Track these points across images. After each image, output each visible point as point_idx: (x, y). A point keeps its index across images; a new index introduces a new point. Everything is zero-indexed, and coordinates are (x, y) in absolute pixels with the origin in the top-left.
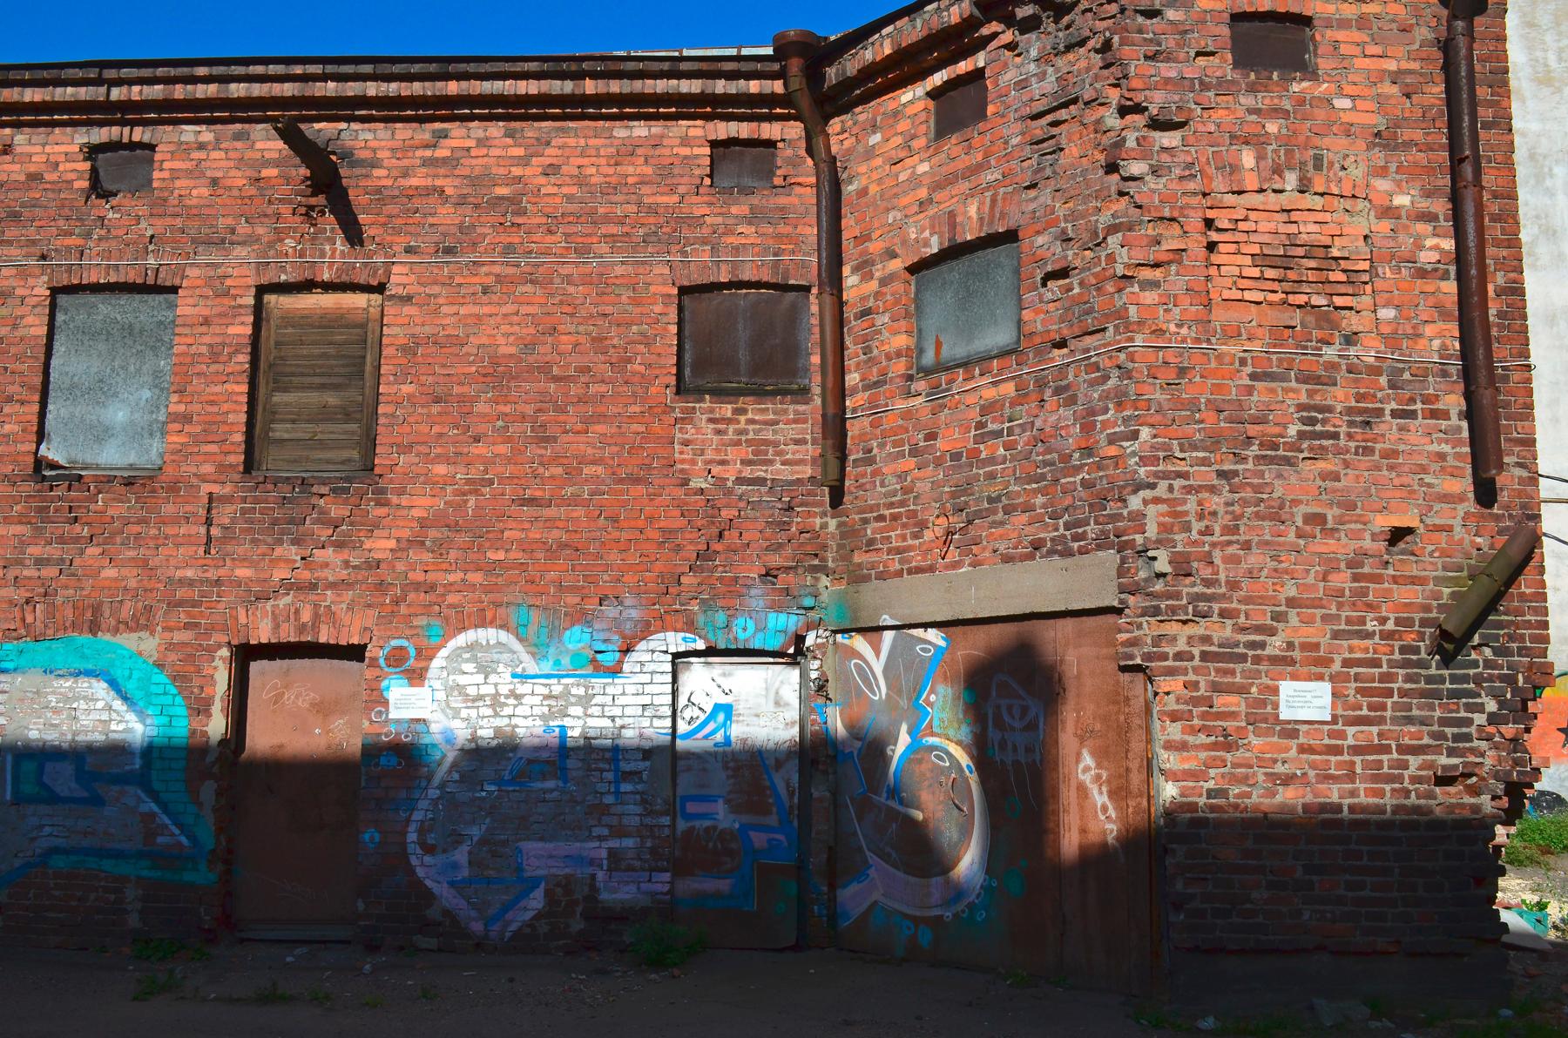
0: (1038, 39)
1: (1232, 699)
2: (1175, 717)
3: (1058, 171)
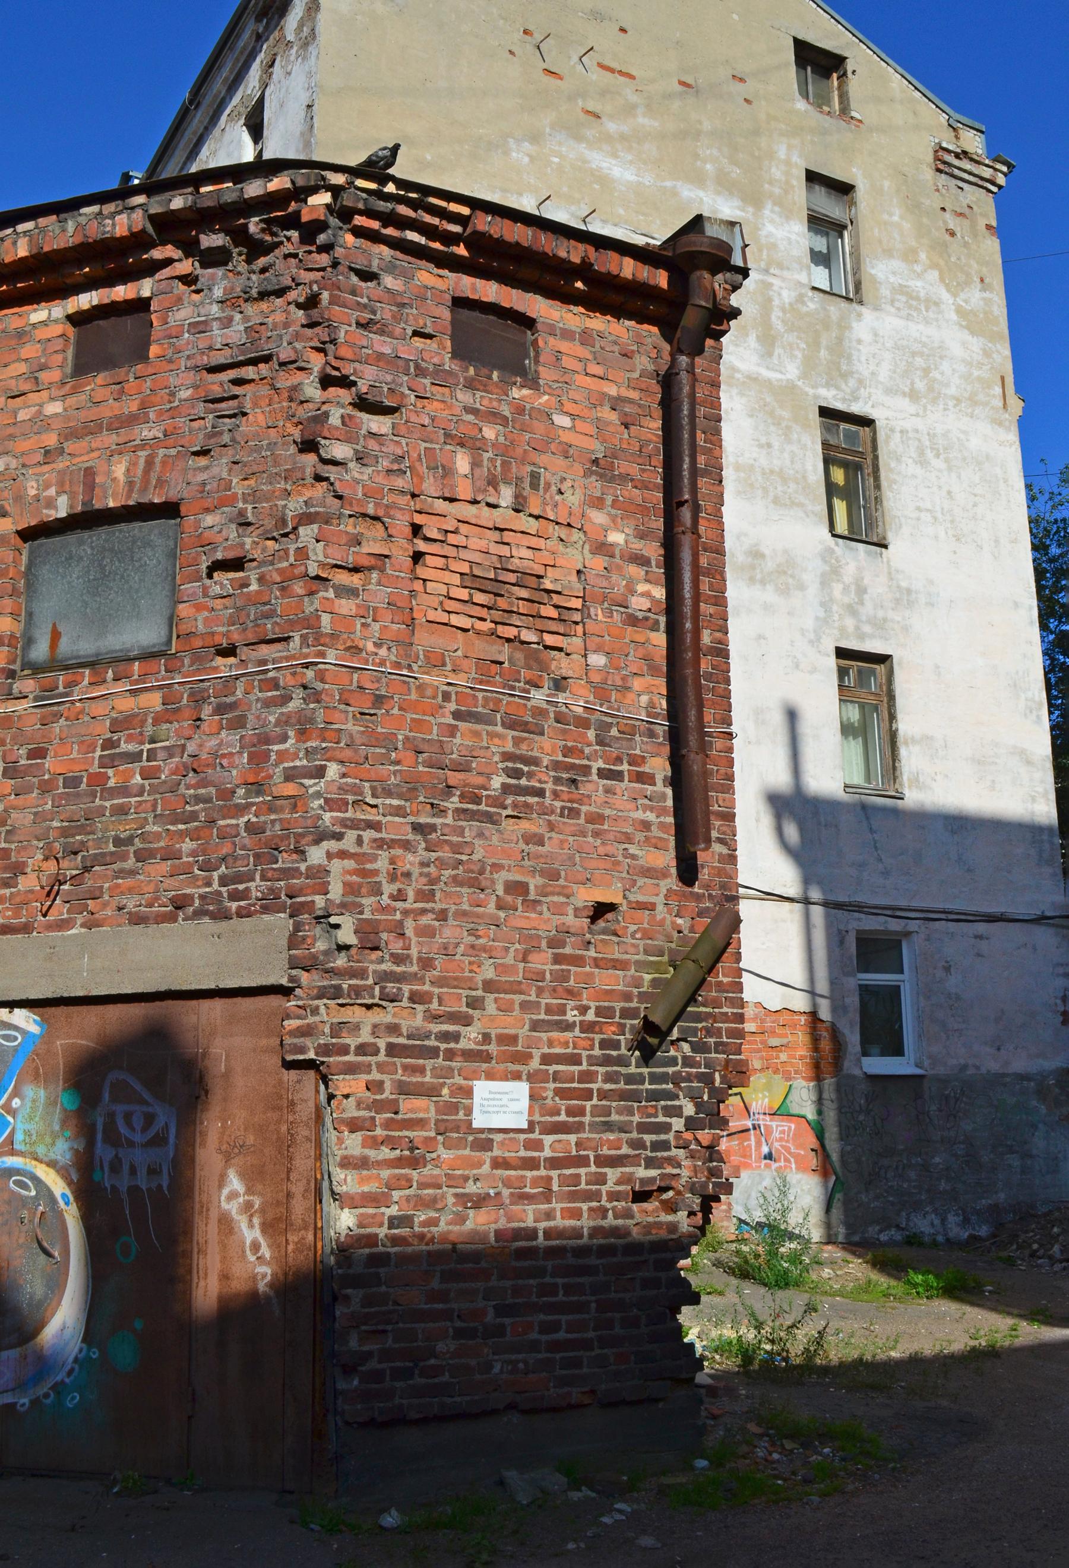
0: (224, 277)
1: (420, 1102)
2: (354, 1126)
3: (239, 438)
